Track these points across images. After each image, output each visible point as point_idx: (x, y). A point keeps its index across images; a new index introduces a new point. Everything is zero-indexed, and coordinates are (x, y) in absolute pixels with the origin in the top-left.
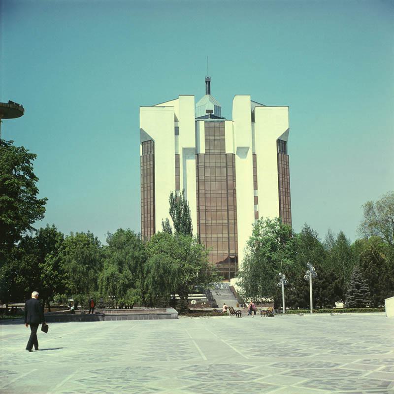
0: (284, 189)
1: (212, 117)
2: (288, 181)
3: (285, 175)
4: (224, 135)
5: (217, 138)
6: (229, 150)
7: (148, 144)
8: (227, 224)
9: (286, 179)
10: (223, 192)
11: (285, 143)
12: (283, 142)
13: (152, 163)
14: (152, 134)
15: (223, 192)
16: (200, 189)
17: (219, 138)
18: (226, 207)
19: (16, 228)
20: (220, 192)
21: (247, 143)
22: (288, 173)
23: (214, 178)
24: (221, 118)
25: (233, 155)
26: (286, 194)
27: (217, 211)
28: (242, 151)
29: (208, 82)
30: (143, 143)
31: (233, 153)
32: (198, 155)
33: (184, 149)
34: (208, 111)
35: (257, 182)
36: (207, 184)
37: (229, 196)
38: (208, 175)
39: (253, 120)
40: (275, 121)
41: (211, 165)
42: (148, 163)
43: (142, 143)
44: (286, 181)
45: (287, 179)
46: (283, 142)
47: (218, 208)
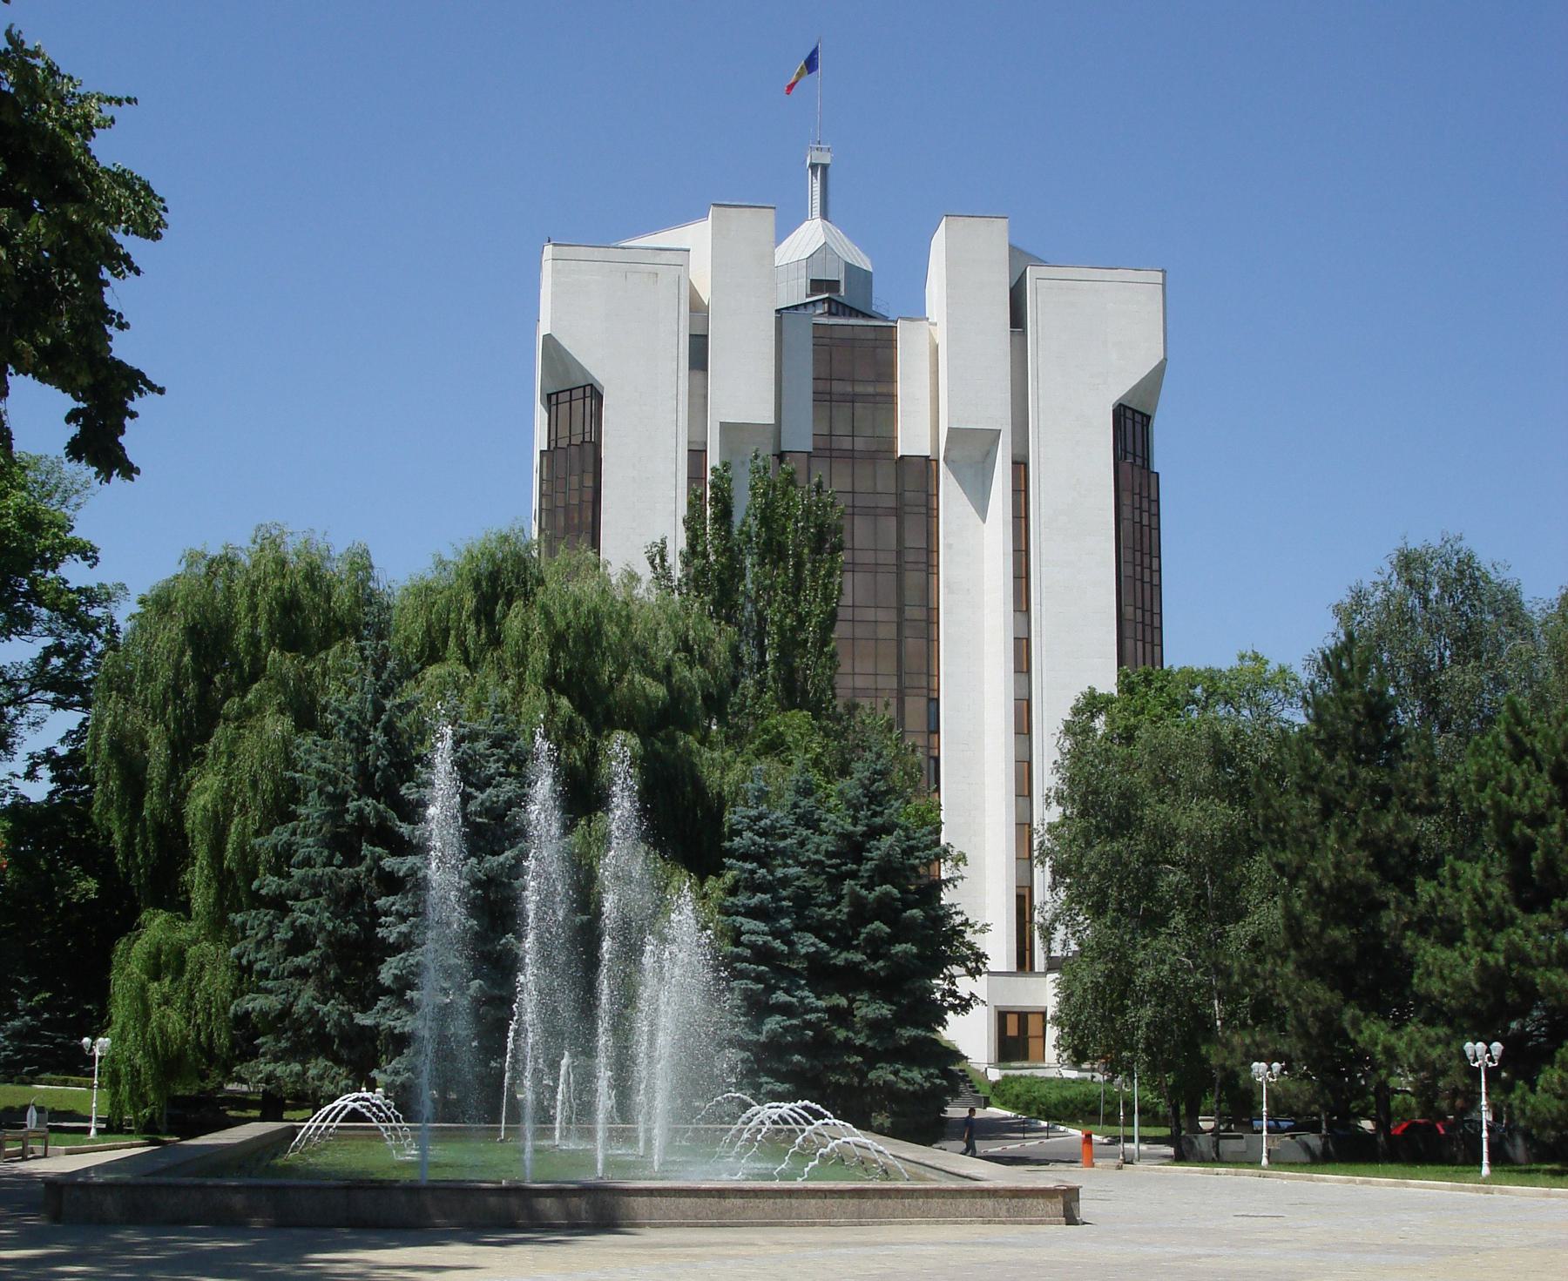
0: (1139, 612)
4: (890, 378)
5: (859, 389)
7: (576, 401)
9: (1147, 572)
10: (882, 615)
11: (1147, 419)
13: (589, 483)
14: (595, 362)
17: (870, 390)
18: (895, 679)
19: (46, 1016)
20: (869, 614)
21: (994, 414)
25: (927, 465)
26: (1148, 634)
28: (973, 449)
29: (811, 64)
30: (551, 400)
31: (928, 453)
33: (725, 428)
37: (907, 632)
40: (1106, 331)
42: (575, 480)
43: (549, 396)
46: (1138, 418)
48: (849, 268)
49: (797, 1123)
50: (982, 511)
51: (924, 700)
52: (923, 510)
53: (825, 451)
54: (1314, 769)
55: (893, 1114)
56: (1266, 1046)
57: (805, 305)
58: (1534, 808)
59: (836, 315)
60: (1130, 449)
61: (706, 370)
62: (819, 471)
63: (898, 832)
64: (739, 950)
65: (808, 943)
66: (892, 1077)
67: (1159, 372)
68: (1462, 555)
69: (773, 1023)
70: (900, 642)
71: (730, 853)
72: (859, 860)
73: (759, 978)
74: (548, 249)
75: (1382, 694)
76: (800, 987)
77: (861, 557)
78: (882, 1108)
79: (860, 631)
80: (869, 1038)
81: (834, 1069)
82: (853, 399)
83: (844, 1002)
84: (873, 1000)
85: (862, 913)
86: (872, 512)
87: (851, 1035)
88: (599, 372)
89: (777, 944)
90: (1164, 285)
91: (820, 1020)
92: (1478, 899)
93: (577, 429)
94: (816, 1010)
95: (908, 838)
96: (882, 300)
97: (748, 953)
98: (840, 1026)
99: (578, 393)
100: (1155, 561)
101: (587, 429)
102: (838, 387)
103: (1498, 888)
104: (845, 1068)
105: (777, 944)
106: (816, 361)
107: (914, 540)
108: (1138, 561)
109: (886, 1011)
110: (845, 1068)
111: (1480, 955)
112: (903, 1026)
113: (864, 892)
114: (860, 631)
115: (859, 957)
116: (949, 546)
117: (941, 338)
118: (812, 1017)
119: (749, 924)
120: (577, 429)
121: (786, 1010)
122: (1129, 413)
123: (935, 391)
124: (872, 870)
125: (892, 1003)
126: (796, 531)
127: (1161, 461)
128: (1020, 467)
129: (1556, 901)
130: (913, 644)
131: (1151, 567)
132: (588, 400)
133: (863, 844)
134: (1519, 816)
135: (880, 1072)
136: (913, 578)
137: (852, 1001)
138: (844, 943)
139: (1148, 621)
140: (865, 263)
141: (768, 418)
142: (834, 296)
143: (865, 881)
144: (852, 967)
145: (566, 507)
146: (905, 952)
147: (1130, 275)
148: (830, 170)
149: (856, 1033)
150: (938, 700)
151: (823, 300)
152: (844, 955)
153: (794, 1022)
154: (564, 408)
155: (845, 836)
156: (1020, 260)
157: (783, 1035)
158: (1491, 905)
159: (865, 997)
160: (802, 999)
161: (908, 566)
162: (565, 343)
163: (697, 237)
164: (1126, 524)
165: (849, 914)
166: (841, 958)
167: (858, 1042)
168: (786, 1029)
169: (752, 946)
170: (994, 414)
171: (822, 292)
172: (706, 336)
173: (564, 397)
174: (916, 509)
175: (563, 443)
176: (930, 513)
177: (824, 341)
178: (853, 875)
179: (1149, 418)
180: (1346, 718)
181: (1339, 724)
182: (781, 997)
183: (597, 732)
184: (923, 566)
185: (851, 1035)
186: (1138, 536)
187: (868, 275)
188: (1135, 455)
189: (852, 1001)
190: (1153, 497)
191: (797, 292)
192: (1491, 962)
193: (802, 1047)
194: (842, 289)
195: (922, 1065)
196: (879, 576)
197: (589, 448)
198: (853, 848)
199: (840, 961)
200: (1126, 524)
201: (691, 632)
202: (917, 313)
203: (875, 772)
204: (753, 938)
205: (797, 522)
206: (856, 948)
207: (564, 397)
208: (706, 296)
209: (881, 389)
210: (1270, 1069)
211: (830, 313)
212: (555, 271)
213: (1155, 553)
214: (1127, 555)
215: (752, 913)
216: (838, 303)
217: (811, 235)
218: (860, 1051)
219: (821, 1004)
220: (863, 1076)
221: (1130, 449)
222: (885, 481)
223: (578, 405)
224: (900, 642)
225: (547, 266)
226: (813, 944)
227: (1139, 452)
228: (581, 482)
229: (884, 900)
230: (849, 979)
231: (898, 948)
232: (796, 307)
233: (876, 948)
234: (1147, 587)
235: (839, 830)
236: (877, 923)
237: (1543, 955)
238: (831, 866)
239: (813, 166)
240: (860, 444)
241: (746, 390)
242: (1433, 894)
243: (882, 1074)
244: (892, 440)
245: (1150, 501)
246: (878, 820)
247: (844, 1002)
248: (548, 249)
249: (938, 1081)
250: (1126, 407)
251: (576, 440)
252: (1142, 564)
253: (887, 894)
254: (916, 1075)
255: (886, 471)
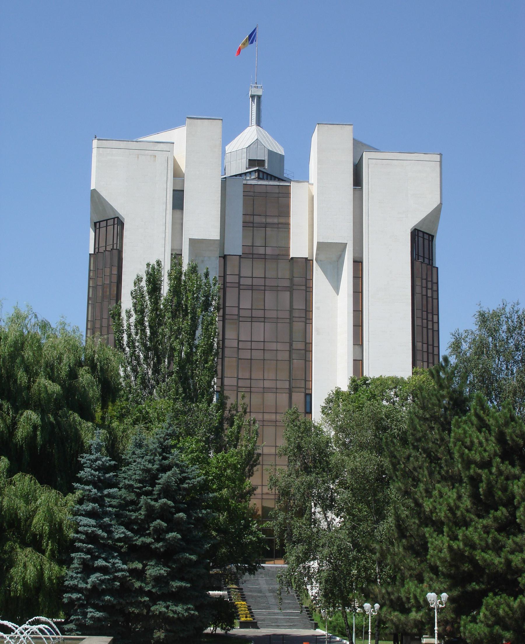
0: (425, 346)
1: (263, 175)
2: (435, 328)
3: (427, 313)
4: (287, 214)
5: (269, 220)
6: (299, 247)
7: (109, 227)
8: (288, 321)
9: (430, 323)
10: (280, 347)
11: (432, 237)
12: (426, 237)
13: (115, 271)
14: (120, 205)
15: (280, 347)
16: (227, 336)
17: (275, 220)
18: (287, 383)
20: (273, 346)
22: (435, 309)
23: (260, 313)
24: (280, 179)
25: (307, 262)
27: (265, 390)
28: (331, 253)
29: (252, 38)
30: (96, 225)
31: (306, 256)
32: (224, 257)
33: (193, 242)
34: (252, 163)
35: (290, 336)
36: (246, 295)
37: (294, 356)
38: (246, 304)
39: (358, 181)
40: (407, 189)
41: (256, 282)
42: (107, 271)
43: (95, 224)
44: (430, 327)
45: (433, 291)
46: (426, 237)
47: (267, 384)
48: (271, 153)
49: (51, 634)
50: (337, 288)
51: (303, 395)
52: (304, 288)
53: (249, 255)
54: (420, 435)
55: (167, 631)
56: (393, 594)
57: (245, 174)
58: (482, 458)
59: (262, 179)
60: (421, 254)
61: (182, 209)
62: (246, 265)
63: (175, 469)
64: (78, 536)
65: (120, 532)
66: (164, 609)
67: (437, 211)
68: (520, 313)
69: (94, 578)
70: (290, 360)
71: (80, 481)
72: (153, 485)
73: (89, 551)
74: (95, 143)
75: (461, 393)
76: (114, 557)
77: (268, 314)
78: (160, 628)
79: (268, 356)
80: (153, 587)
81: (131, 604)
82: (266, 226)
83: (140, 566)
84: (157, 565)
85: (152, 514)
86: (276, 289)
87: (143, 585)
88: (122, 211)
89: (100, 532)
90: (441, 162)
91: (125, 577)
92: (451, 509)
93: (110, 242)
94: (122, 570)
95: (182, 472)
96: (288, 171)
97: (83, 537)
98: (138, 580)
99: (110, 222)
100: (435, 317)
101: (115, 242)
102: (257, 219)
103: (467, 502)
104: (138, 604)
105: (100, 532)
106: (245, 204)
107: (299, 305)
108: (425, 317)
109: (163, 571)
110: (138, 604)
111: (448, 542)
112: (173, 580)
113: (153, 503)
114: (268, 356)
115: (149, 540)
116: (318, 308)
117: (315, 193)
118: (119, 574)
119: (86, 520)
120: (110, 242)
121: (104, 570)
122: (421, 234)
123: (312, 219)
124: (160, 490)
125: (168, 567)
126: (193, 299)
127: (439, 261)
128: (358, 263)
129: (492, 512)
130: (297, 363)
131: (432, 321)
132: (116, 226)
133: (157, 475)
134: (475, 463)
135: (157, 607)
136: (298, 326)
137: (145, 566)
138: (141, 531)
139: (430, 350)
140: (280, 150)
141: (215, 234)
142: (261, 169)
143: (156, 497)
144: (146, 546)
145: (103, 285)
146: (172, 537)
147: (422, 156)
148: (262, 98)
149: (147, 584)
150: (311, 395)
151: (255, 171)
152: (143, 539)
153: (107, 577)
154: (103, 230)
155: (147, 471)
156: (359, 147)
157: (100, 585)
158: (459, 513)
159: (153, 563)
160: (114, 564)
161: (294, 319)
162: (104, 194)
163: (178, 136)
164: (418, 297)
165: (145, 515)
166: (139, 541)
167: (147, 589)
168: (102, 581)
169: (86, 533)
170: (344, 234)
171: (255, 167)
172: (183, 191)
173: (103, 224)
174: (299, 287)
175: (102, 250)
176: (308, 290)
177: (250, 194)
178: (148, 493)
179: (432, 237)
180: (440, 406)
181: (436, 409)
182: (100, 563)
183: (16, 412)
184: (304, 319)
185: (143, 585)
186: (425, 302)
187: (282, 157)
188: (424, 257)
189: (145, 566)
190: (435, 281)
191: (239, 166)
192: (455, 547)
193: (111, 592)
194: (266, 165)
195: (185, 603)
196: (279, 325)
197: (115, 252)
198: (151, 478)
199: (139, 543)
200: (418, 297)
201: (96, 356)
202: (305, 178)
203: (167, 435)
204: (86, 529)
205: (194, 294)
206: (149, 535)
207: (103, 224)
208: (183, 168)
209: (282, 220)
210: (373, 607)
211: (259, 178)
212: (99, 154)
213: (435, 312)
214: (418, 313)
215: (90, 514)
216: (263, 172)
217: (250, 134)
218: (149, 594)
219: (125, 567)
220: (148, 607)
221: (421, 254)
222: (284, 271)
223: (110, 228)
224: (290, 360)
225: (95, 151)
226: (123, 533)
227: (426, 256)
228: (111, 271)
229: (164, 507)
230: (144, 553)
231: (171, 535)
232: (240, 175)
233: (159, 535)
234: (430, 332)
235: (142, 467)
236: (158, 521)
237: (483, 543)
238: (137, 488)
239: (253, 97)
240: (269, 251)
241: (204, 221)
242: (431, 506)
243: (159, 608)
244: (287, 249)
245: (432, 283)
246: (166, 462)
247: (140, 566)
248: (95, 143)
249: (192, 612)
250: (418, 230)
251: (109, 248)
252: (427, 319)
253: (165, 504)
254: (179, 609)
255: (284, 266)
